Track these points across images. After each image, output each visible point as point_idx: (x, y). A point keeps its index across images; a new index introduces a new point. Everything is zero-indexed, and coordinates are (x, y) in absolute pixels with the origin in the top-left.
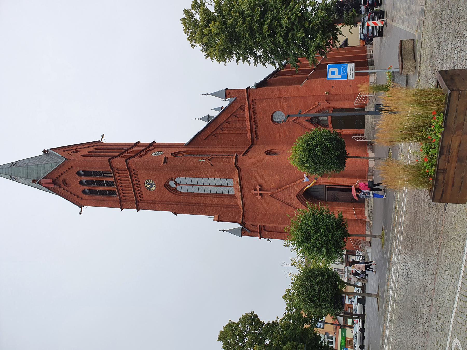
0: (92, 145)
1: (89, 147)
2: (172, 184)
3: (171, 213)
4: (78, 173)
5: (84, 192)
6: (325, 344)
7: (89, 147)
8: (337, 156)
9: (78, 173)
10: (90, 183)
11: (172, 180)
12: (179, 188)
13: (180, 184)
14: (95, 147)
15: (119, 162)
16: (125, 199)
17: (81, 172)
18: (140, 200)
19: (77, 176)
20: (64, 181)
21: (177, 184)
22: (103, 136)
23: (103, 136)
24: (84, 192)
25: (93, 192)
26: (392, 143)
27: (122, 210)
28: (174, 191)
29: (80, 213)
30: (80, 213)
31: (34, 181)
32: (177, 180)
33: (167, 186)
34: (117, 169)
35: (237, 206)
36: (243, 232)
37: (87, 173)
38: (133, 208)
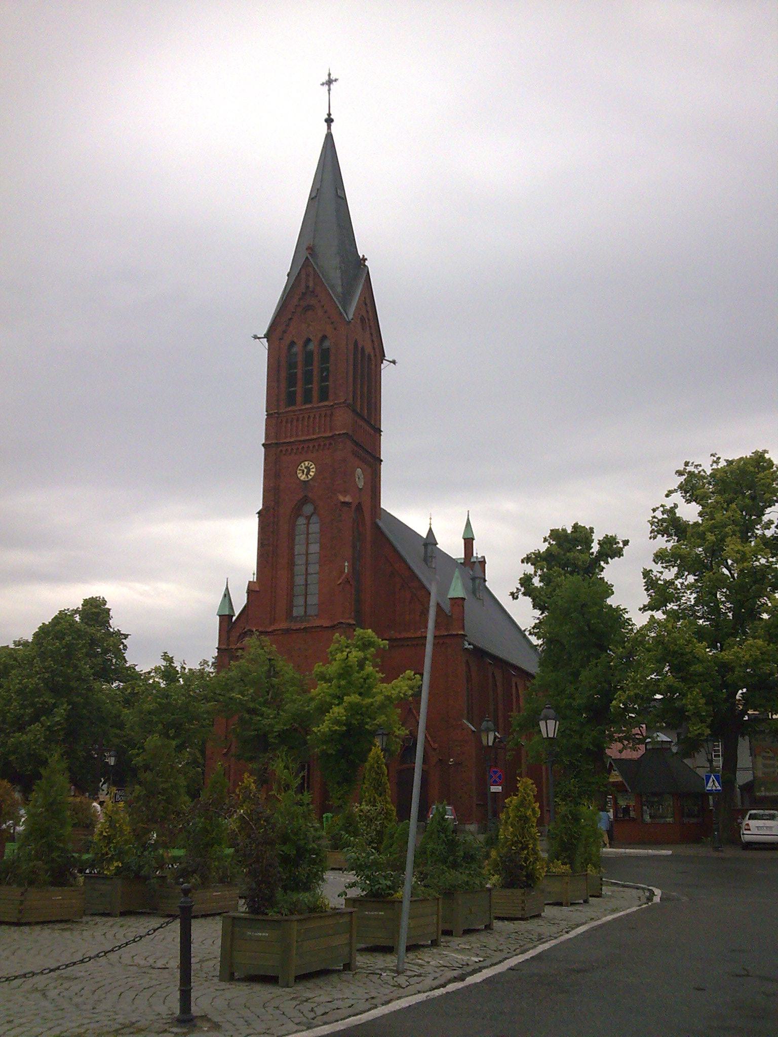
0: (375, 339)
1: (373, 341)
2: (308, 509)
3: (260, 507)
4: (324, 337)
5: (293, 344)
6: (353, 885)
7: (373, 341)
8: (254, 909)
9: (324, 337)
10: (309, 356)
11: (315, 509)
12: (301, 521)
13: (308, 524)
14: (372, 355)
15: (343, 420)
16: (281, 422)
17: (326, 344)
18: (281, 451)
19: (320, 336)
20: (309, 308)
21: (308, 518)
22: (394, 362)
23: (394, 362)
24: (293, 344)
25: (292, 365)
26: (447, 927)
27: (263, 445)
28: (297, 511)
29: (256, 337)
30: (256, 337)
31: (311, 249)
32: (314, 519)
33: (305, 500)
34: (332, 415)
35: (273, 621)
36: (226, 620)
37: (325, 354)
38: (266, 439)
